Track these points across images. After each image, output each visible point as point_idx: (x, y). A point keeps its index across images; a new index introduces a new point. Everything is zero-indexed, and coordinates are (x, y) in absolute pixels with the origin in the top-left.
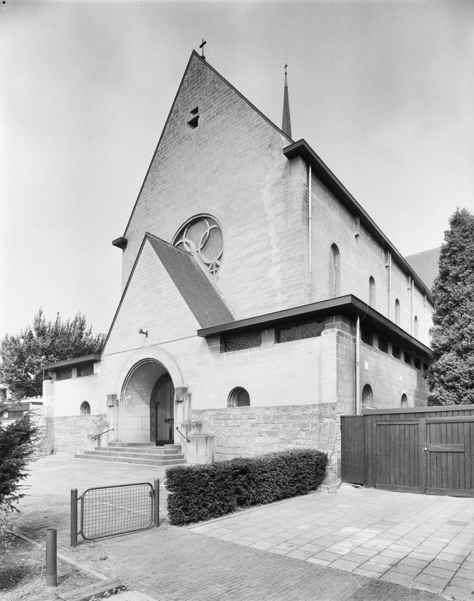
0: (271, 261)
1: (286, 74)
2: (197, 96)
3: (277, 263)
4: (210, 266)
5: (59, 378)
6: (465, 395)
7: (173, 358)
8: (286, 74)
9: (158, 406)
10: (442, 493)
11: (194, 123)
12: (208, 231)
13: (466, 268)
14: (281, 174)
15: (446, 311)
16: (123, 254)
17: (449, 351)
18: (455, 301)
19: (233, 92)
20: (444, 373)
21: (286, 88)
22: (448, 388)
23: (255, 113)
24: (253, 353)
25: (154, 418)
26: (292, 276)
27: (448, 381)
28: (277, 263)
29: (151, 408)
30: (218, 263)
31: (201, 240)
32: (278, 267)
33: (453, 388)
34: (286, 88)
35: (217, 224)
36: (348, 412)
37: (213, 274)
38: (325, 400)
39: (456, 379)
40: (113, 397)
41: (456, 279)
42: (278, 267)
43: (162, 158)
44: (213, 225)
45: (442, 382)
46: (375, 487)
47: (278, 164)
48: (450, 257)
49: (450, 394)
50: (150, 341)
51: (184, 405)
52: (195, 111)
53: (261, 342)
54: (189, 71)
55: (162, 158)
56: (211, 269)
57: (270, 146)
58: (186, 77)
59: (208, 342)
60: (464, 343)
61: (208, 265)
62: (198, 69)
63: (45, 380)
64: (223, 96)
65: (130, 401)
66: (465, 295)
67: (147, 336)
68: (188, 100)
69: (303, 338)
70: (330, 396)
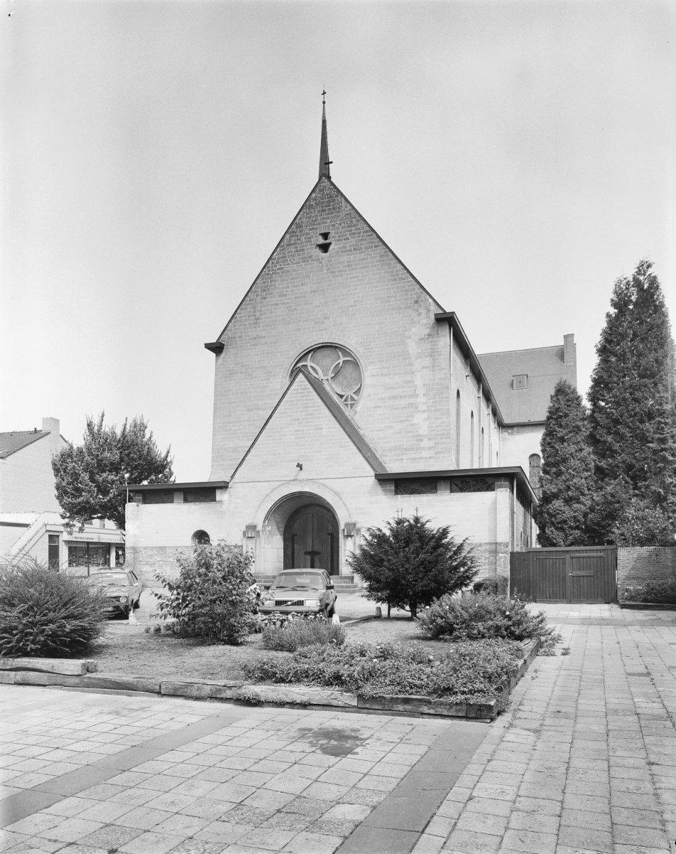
0: (417, 408)
1: (324, 103)
2: (329, 221)
3: (424, 411)
4: (344, 399)
5: (145, 501)
6: (571, 535)
7: (336, 494)
8: (324, 103)
9: (295, 537)
10: (580, 602)
11: (325, 248)
12: (341, 361)
13: (570, 432)
14: (427, 331)
15: (556, 464)
16: (216, 362)
17: (558, 499)
18: (562, 458)
19: (375, 236)
20: (555, 516)
21: (324, 122)
22: (557, 529)
23: (399, 266)
24: (430, 498)
25: (290, 549)
26: (440, 426)
27: (558, 523)
28: (424, 411)
29: (285, 541)
30: (354, 396)
31: (332, 368)
32: (425, 415)
33: (562, 529)
34: (324, 122)
35: (351, 356)
36: (517, 549)
37: (347, 407)
38: (499, 540)
39: (565, 522)
40: (252, 527)
41: (562, 440)
42: (425, 415)
43: (279, 269)
44: (347, 356)
45: (553, 524)
46: (536, 602)
47: (424, 321)
48: (556, 419)
49: (560, 534)
50: (303, 475)
51: (355, 540)
52: (325, 236)
53: (437, 490)
54: (317, 190)
55: (279, 269)
56: (345, 400)
57: (416, 302)
58: (314, 195)
59: (380, 484)
60: (570, 493)
61: (341, 396)
62: (326, 194)
63: (129, 501)
64: (362, 234)
65: (270, 532)
66: (570, 454)
67: (301, 469)
68: (316, 220)
69: (474, 491)
70: (503, 536)
